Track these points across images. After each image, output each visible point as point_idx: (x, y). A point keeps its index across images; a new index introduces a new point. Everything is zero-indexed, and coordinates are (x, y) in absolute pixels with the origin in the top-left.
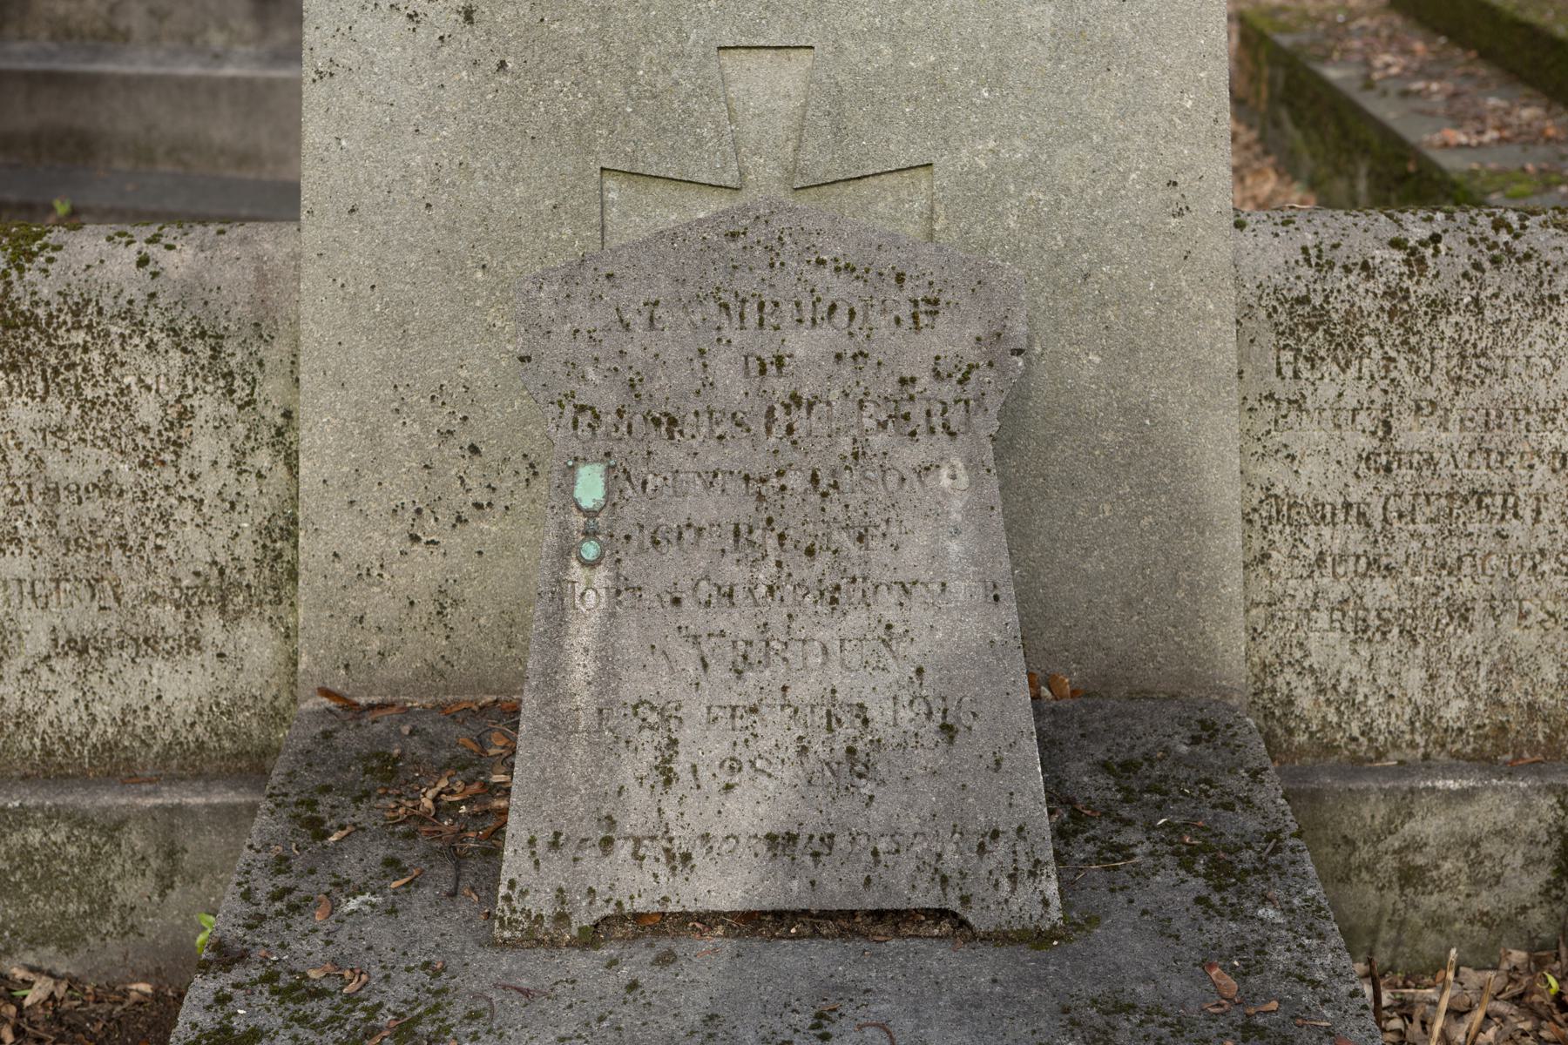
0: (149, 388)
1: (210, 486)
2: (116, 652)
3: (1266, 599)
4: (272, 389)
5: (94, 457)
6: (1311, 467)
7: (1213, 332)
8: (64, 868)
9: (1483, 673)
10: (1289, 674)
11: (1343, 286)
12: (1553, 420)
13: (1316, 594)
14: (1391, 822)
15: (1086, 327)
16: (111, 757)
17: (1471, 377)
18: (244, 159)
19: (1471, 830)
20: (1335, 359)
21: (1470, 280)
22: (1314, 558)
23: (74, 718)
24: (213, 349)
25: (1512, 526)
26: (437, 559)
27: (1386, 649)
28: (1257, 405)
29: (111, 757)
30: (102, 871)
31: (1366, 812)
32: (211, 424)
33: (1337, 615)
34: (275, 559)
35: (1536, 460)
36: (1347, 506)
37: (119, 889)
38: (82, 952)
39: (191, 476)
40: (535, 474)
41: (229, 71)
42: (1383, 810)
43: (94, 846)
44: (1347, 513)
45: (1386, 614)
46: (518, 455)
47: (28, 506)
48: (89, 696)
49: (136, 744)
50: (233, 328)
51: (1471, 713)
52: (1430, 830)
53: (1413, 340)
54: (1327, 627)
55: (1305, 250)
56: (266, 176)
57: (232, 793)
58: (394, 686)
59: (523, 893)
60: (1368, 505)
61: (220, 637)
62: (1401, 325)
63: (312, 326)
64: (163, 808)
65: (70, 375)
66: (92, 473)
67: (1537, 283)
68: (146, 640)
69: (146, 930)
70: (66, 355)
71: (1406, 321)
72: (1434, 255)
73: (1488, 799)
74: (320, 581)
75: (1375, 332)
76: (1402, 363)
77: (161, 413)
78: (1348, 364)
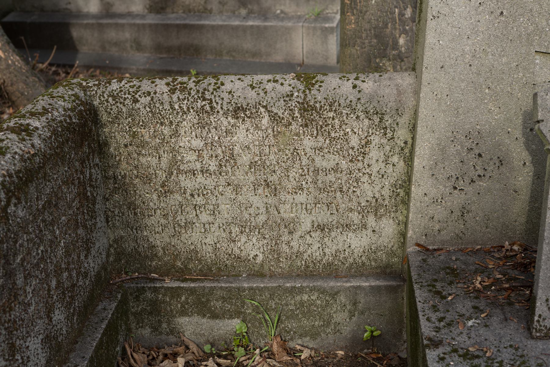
0: (355, 133)
1: (375, 169)
2: (335, 230)
5: (333, 158)
8: (315, 309)
16: (330, 268)
18: (254, 55)
23: (318, 254)
24: (380, 119)
26: (463, 196)
29: (330, 268)
30: (329, 310)
32: (377, 146)
34: (397, 196)
37: (335, 317)
38: (319, 339)
39: (368, 165)
40: (502, 164)
41: (250, 23)
43: (327, 301)
46: (496, 157)
47: (307, 176)
48: (324, 246)
49: (340, 263)
50: (388, 111)
56: (263, 61)
57: (378, 282)
58: (443, 242)
59: (544, 319)
61: (374, 224)
63: (424, 110)
64: (353, 287)
65: (327, 128)
66: (332, 164)
68: (347, 225)
69: (343, 331)
70: (326, 121)
74: (418, 204)
77: (359, 142)
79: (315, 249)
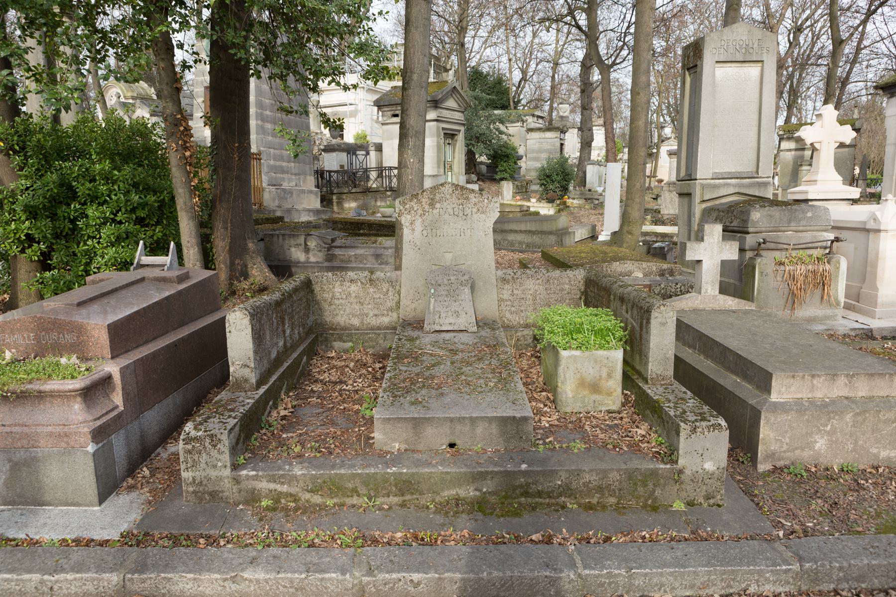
4: (398, 287)
79: (374, 322)
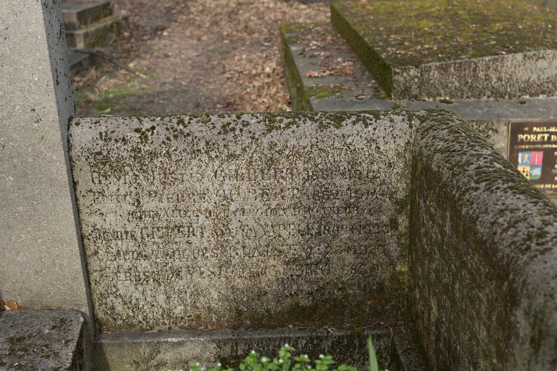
3: (99, 269)
6: (110, 218)
7: (57, 167)
9: (188, 296)
10: (112, 298)
11: (115, 147)
12: (204, 198)
13: (118, 267)
14: (152, 355)
15: (6, 166)
17: (169, 182)
19: (184, 357)
20: (115, 176)
21: (165, 144)
22: (116, 253)
25: (192, 239)
27: (148, 287)
28: (86, 194)
31: (141, 351)
33: (128, 274)
35: (199, 214)
36: (127, 233)
42: (148, 350)
44: (127, 235)
45: (147, 274)
51: (185, 312)
52: (168, 358)
53: (145, 168)
54: (124, 279)
55: (101, 134)
60: (135, 232)
62: (139, 162)
67: (192, 145)
71: (141, 160)
72: (152, 135)
73: (189, 345)
75: (129, 165)
76: (141, 177)
78: (120, 178)
